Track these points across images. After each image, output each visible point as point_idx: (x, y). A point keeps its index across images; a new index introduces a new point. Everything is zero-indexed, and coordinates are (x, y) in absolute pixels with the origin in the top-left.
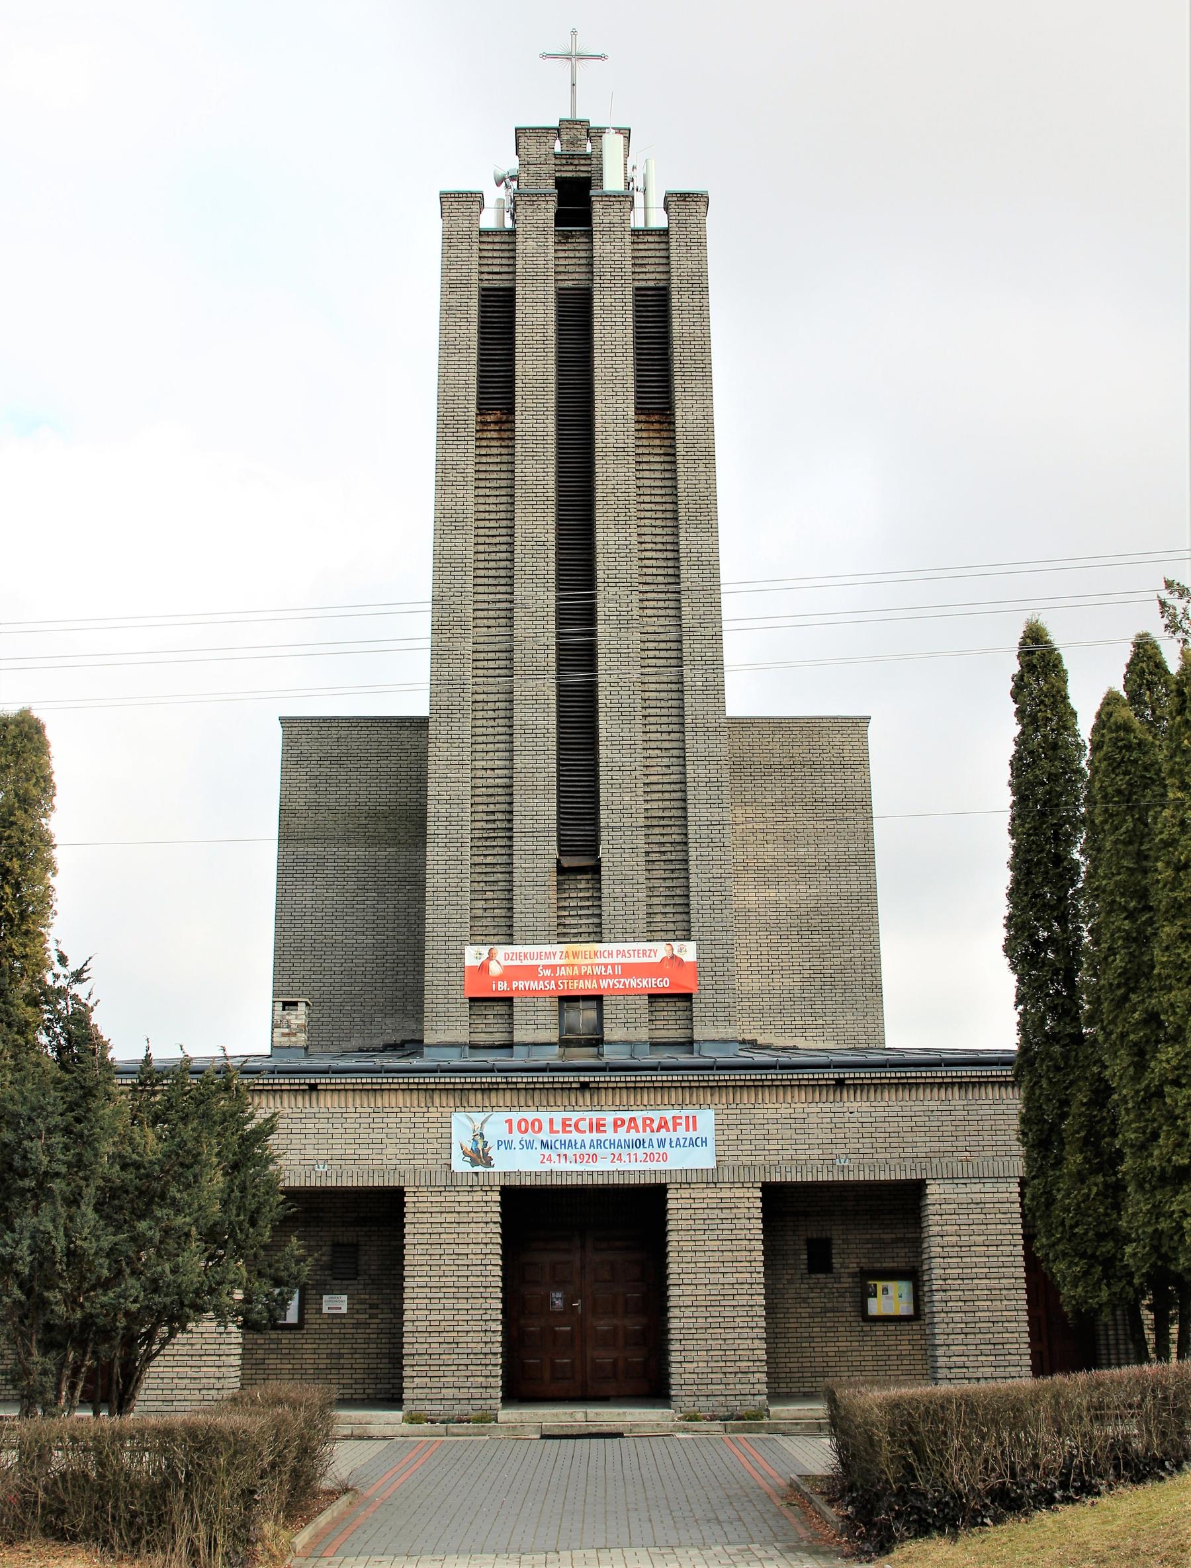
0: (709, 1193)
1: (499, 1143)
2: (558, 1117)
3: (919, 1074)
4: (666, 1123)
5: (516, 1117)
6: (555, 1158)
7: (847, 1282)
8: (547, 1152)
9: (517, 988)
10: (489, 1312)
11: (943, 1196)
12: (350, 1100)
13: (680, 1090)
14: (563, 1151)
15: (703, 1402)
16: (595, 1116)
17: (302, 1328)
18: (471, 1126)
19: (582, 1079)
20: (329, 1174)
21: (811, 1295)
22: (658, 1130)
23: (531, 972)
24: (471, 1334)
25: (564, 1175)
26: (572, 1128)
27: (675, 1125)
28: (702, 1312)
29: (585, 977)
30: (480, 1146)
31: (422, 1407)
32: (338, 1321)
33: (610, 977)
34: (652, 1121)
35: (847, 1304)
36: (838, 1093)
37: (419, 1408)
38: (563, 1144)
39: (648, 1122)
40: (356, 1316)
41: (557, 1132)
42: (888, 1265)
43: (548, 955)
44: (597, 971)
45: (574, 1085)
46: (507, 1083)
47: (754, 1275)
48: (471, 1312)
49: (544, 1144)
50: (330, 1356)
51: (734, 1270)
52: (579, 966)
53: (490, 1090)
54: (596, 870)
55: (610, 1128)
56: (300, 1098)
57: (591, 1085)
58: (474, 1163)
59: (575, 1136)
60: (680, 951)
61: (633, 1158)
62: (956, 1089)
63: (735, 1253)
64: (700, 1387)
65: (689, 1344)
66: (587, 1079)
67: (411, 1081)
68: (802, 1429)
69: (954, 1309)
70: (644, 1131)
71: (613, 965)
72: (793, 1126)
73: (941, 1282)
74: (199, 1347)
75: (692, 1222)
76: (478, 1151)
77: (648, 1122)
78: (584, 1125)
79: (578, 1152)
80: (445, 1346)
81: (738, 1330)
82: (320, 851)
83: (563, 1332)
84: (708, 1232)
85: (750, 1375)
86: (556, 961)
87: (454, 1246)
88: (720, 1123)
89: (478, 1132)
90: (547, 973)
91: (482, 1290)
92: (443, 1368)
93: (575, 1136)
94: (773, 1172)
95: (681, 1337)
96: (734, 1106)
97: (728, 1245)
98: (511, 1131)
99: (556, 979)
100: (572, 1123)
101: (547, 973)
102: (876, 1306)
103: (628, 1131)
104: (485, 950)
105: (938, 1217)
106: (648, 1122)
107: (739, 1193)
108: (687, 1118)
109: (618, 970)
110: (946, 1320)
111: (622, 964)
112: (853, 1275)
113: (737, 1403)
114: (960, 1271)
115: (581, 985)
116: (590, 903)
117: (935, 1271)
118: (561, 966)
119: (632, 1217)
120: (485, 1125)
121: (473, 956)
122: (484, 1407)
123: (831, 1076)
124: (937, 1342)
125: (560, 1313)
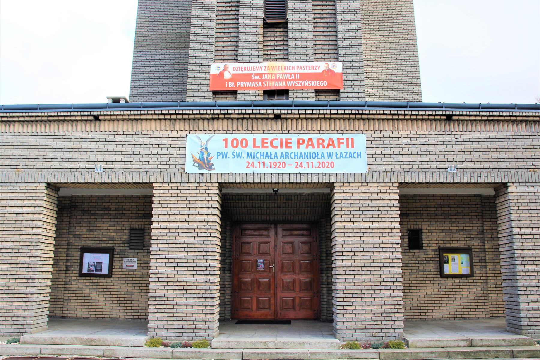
0: (363, 189)
1: (218, 154)
2: (259, 138)
3: (501, 114)
4: (333, 142)
5: (230, 137)
6: (256, 164)
7: (431, 254)
8: (251, 160)
9: (240, 86)
10: (209, 269)
11: (519, 194)
12: (120, 126)
13: (342, 121)
14: (262, 160)
15: (359, 333)
16: (284, 137)
17: (112, 277)
18: (200, 143)
19: (275, 112)
20: (104, 174)
21: (410, 262)
22: (328, 147)
23: (248, 77)
24: (196, 284)
25: (263, 176)
26: (269, 145)
27: (339, 144)
28: (358, 271)
29: (279, 80)
30: (205, 156)
31: (161, 334)
32: (132, 273)
33: (293, 80)
34: (323, 140)
35: (432, 267)
36: (447, 125)
37: (159, 334)
38: (262, 155)
39: (321, 141)
40: (142, 271)
41: (259, 147)
42: (455, 245)
43: (258, 68)
44: (286, 77)
45: (270, 116)
46: (224, 114)
47: (395, 246)
48: (196, 269)
49: (249, 155)
50: (127, 293)
51: (381, 242)
52: (276, 74)
53: (213, 119)
54: (285, 25)
55: (294, 145)
56: (88, 125)
57: (282, 116)
58: (200, 167)
59: (270, 150)
60: (333, 66)
61: (310, 165)
62: (524, 124)
63: (381, 231)
64: (357, 323)
65: (349, 293)
66: (279, 112)
67: (160, 112)
68: (436, 357)
69: (530, 270)
70: (318, 147)
71: (295, 74)
72: (419, 146)
73: (520, 252)
74: (13, 288)
75: (351, 209)
76: (203, 160)
77: (320, 142)
78: (277, 143)
79: (272, 161)
80: (177, 291)
81: (383, 284)
82: (153, 51)
83: (264, 282)
84: (362, 216)
85: (392, 315)
86: (263, 71)
87: (186, 223)
88: (370, 143)
89: (204, 147)
90: (257, 78)
91: (204, 254)
92: (176, 307)
93: (270, 150)
94: (406, 175)
95: (344, 288)
96: (379, 132)
97: (376, 225)
98: (226, 146)
99: (262, 81)
100: (269, 141)
101: (257, 78)
102: (448, 269)
103: (307, 147)
104: (222, 65)
105: (516, 208)
106: (320, 142)
107: (384, 190)
108: (347, 139)
109: (298, 77)
110: (525, 277)
111: (300, 73)
112: (435, 251)
113: (383, 334)
114: (532, 244)
115: (276, 84)
116: (282, 43)
117: (515, 244)
118: (265, 74)
119: (307, 212)
120: (209, 142)
121: (215, 68)
122: (205, 335)
123: (444, 113)
124: (519, 292)
125: (263, 271)
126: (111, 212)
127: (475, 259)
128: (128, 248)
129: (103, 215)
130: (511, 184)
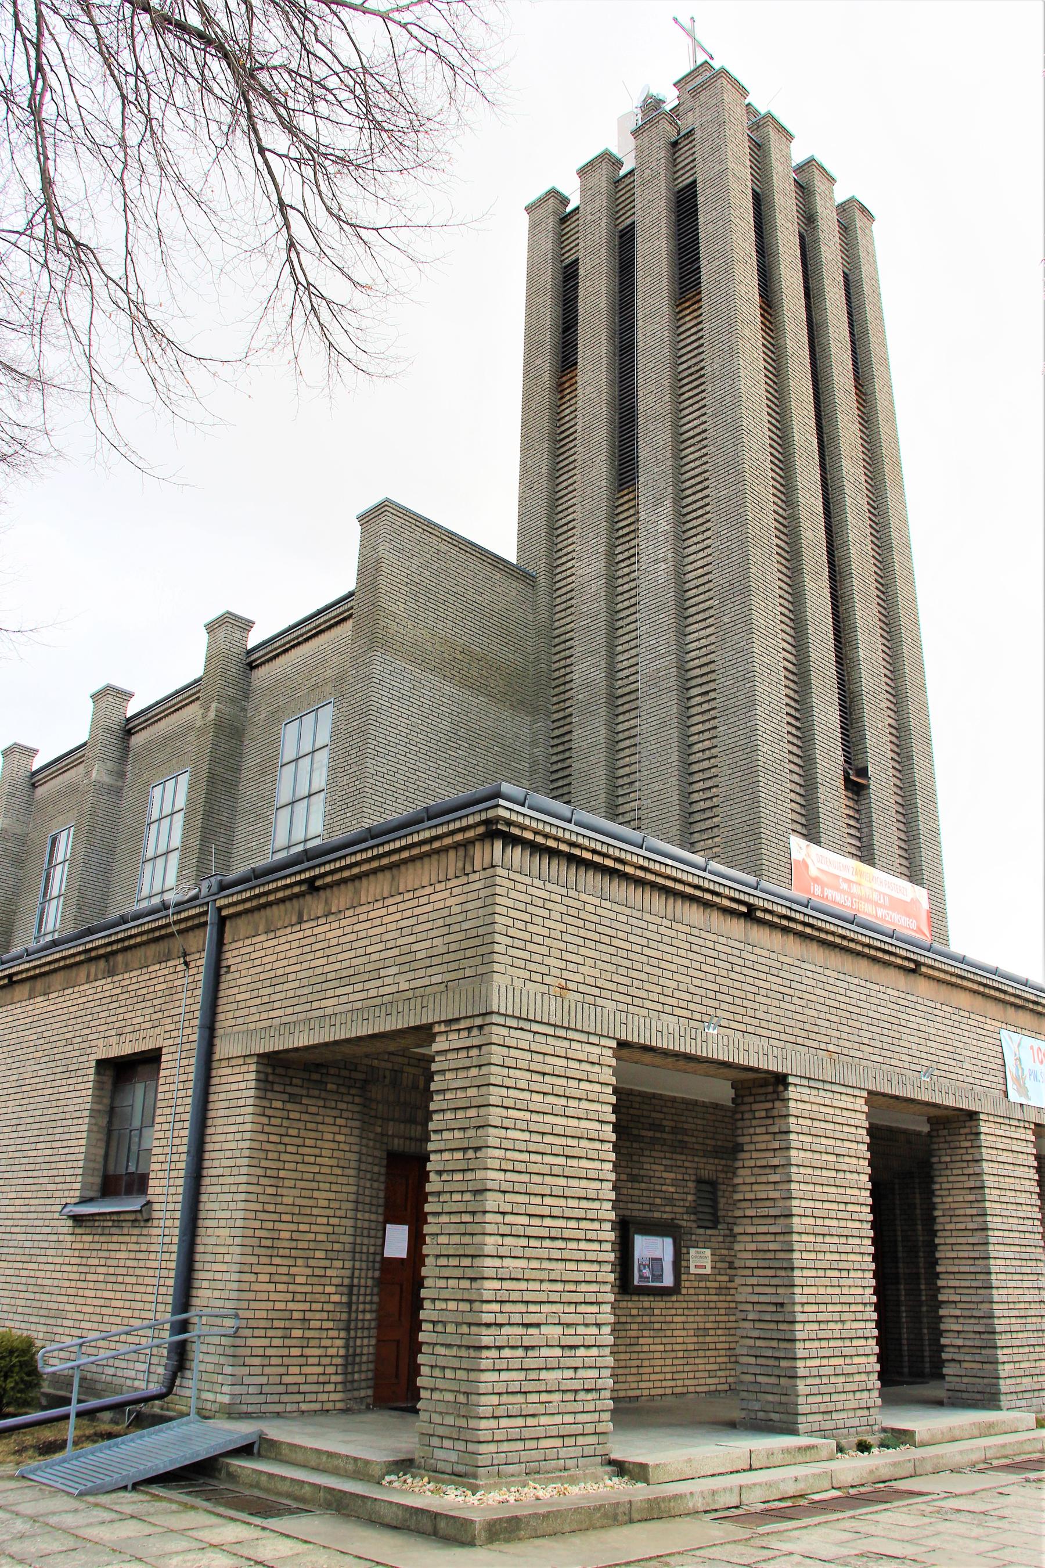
126: (665, 1136)
127: (687, 1284)
128: (694, 1225)
129: (654, 1141)
130: (797, 1081)
